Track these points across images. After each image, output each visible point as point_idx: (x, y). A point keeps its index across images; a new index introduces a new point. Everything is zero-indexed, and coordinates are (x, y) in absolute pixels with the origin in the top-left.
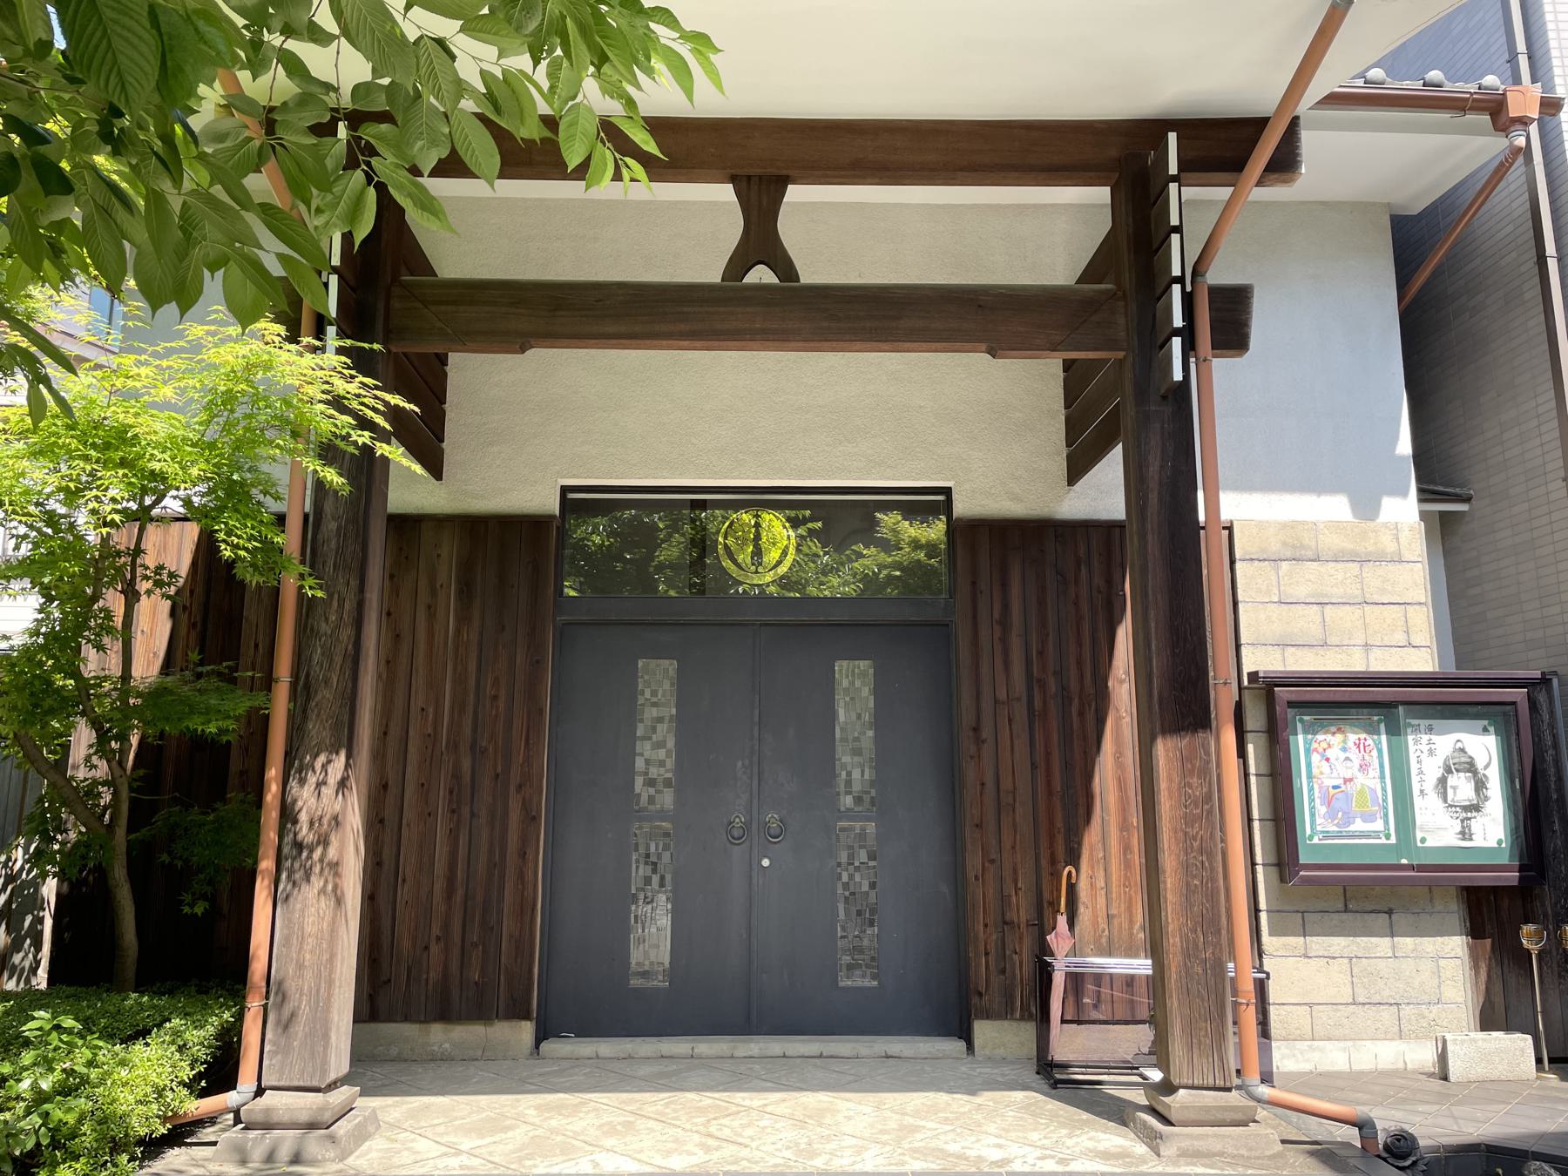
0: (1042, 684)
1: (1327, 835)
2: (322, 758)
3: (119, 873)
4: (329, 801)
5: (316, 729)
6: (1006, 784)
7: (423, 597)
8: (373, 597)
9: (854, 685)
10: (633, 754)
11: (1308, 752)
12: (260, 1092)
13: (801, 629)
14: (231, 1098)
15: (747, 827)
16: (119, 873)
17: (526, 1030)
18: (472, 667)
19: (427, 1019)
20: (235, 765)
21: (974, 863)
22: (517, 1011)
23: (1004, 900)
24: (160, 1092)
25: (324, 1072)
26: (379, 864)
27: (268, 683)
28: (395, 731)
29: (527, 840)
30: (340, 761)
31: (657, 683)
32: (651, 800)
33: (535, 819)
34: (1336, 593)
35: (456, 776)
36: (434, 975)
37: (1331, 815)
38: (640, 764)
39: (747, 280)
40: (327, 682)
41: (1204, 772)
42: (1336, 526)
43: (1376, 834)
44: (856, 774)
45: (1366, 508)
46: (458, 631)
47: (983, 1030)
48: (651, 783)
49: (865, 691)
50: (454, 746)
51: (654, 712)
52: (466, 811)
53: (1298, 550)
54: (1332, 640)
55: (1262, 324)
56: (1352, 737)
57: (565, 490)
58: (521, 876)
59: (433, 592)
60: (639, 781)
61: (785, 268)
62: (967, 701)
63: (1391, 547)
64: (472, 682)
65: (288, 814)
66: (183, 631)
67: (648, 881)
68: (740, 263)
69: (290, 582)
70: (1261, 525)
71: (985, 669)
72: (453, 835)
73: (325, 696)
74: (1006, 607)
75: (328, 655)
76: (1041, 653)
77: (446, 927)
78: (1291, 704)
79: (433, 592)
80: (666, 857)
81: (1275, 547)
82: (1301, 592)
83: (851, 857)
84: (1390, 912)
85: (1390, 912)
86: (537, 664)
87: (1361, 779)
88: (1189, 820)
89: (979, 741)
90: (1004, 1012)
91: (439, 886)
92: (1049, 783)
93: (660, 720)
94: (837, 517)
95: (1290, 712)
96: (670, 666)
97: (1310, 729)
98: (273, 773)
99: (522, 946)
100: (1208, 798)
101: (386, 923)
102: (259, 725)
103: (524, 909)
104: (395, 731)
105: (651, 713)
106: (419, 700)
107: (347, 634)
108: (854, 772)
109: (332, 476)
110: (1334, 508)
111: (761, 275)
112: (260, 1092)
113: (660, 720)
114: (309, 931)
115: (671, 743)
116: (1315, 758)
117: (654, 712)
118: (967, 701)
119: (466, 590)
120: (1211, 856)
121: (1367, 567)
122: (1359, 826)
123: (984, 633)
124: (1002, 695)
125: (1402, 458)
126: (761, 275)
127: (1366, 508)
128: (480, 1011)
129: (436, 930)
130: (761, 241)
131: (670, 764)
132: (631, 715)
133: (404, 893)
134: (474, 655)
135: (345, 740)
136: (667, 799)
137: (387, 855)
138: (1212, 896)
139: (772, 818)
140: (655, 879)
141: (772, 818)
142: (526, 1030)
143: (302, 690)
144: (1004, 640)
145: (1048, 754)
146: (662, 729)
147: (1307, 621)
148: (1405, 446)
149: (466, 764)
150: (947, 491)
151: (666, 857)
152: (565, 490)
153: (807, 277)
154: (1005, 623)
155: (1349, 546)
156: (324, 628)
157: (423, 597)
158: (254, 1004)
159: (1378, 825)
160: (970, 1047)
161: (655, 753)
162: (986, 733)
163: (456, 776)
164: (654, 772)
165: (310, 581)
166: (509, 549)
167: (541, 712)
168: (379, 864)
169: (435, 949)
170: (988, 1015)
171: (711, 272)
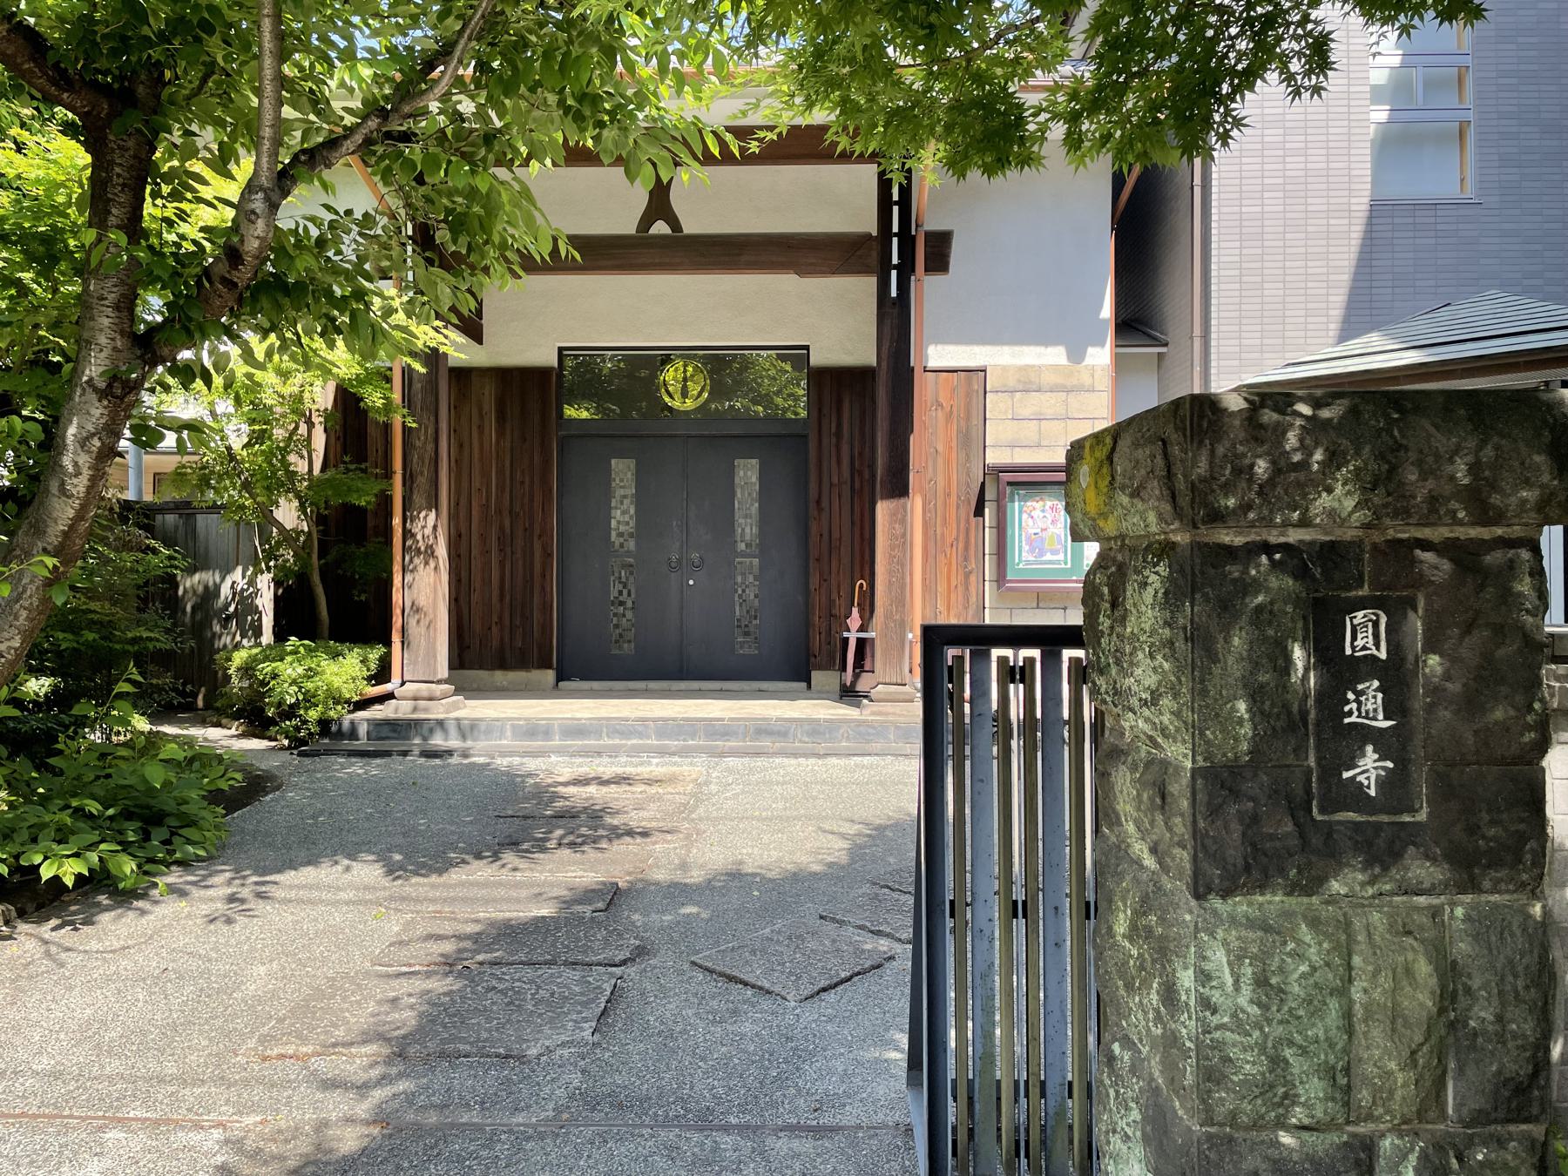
0: (861, 473)
1: (1028, 562)
2: (422, 515)
3: (316, 578)
4: (430, 526)
5: (418, 498)
6: (836, 535)
7: (475, 420)
8: (444, 426)
9: (748, 473)
10: (609, 518)
11: (1020, 512)
12: (403, 684)
13: (716, 437)
14: (388, 687)
15: (679, 561)
16: (316, 578)
17: (550, 675)
18: (508, 463)
19: (493, 668)
20: (371, 523)
21: (814, 581)
22: (545, 664)
23: (831, 603)
24: (354, 679)
25: (435, 674)
26: (459, 581)
27: (388, 475)
28: (463, 501)
29: (546, 566)
30: (433, 515)
31: (623, 471)
32: (622, 545)
33: (550, 555)
34: (1049, 413)
35: (502, 528)
36: (495, 643)
37: (1032, 551)
38: (613, 523)
39: (651, 231)
40: (422, 473)
41: (903, 521)
42: (1055, 368)
43: (1058, 562)
44: (748, 530)
45: (1076, 355)
46: (498, 442)
47: (816, 676)
48: (621, 535)
49: (754, 479)
50: (499, 512)
51: (622, 492)
52: (508, 550)
53: (1028, 384)
54: (1044, 443)
55: (958, 252)
56: (1049, 503)
57: (561, 350)
58: (543, 588)
59: (481, 417)
60: (614, 534)
61: (675, 224)
62: (813, 486)
63: (1087, 381)
64: (508, 473)
65: (407, 534)
66: (333, 440)
67: (621, 593)
68: (646, 221)
69: (397, 420)
70: (1004, 368)
71: (825, 464)
72: (502, 564)
73: (422, 481)
74: (839, 425)
75: (421, 458)
76: (860, 454)
77: (500, 618)
78: (1010, 484)
79: (481, 417)
80: (631, 579)
81: (1012, 383)
82: (1026, 413)
83: (744, 579)
84: (1065, 609)
85: (1065, 609)
86: (547, 463)
87: (1052, 529)
88: (892, 548)
89: (820, 510)
90: (826, 666)
91: (496, 593)
92: (862, 535)
93: (625, 497)
94: (722, 366)
95: (1008, 489)
96: (632, 463)
97: (1023, 499)
98: (397, 521)
99: (546, 627)
100: (904, 535)
101: (465, 612)
102: (385, 501)
103: (546, 608)
104: (463, 501)
105: (619, 492)
106: (476, 483)
107: (430, 447)
108: (747, 526)
109: (419, 367)
110: (1055, 355)
111: (660, 228)
112: (403, 684)
113: (625, 497)
114: (423, 590)
115: (632, 511)
116: (1025, 516)
117: (622, 492)
118: (813, 486)
119: (501, 417)
120: (903, 566)
121: (1071, 395)
122: (1048, 557)
123: (825, 441)
124: (835, 480)
125: (1105, 321)
126: (660, 228)
127: (1076, 355)
128: (523, 663)
129: (495, 619)
130: (660, 202)
131: (632, 524)
132: (608, 493)
133: (475, 597)
134: (508, 457)
135: (433, 503)
136: (631, 545)
137: (464, 574)
138: (903, 587)
139: (695, 556)
140: (625, 592)
141: (695, 556)
142: (550, 675)
143: (409, 480)
144: (838, 447)
145: (862, 515)
146: (626, 502)
147: (1029, 431)
148: (1107, 311)
149: (507, 523)
150: (807, 348)
151: (631, 579)
152: (561, 350)
153: (689, 228)
154: (839, 435)
155: (1060, 380)
156: (418, 443)
157: (475, 420)
158: (396, 638)
159: (1061, 557)
160: (809, 687)
161: (622, 517)
162: (825, 504)
163: (502, 528)
164: (622, 528)
165: (409, 419)
166: (526, 392)
167: (551, 491)
168: (459, 581)
169: (495, 629)
170: (820, 668)
171: (628, 227)
